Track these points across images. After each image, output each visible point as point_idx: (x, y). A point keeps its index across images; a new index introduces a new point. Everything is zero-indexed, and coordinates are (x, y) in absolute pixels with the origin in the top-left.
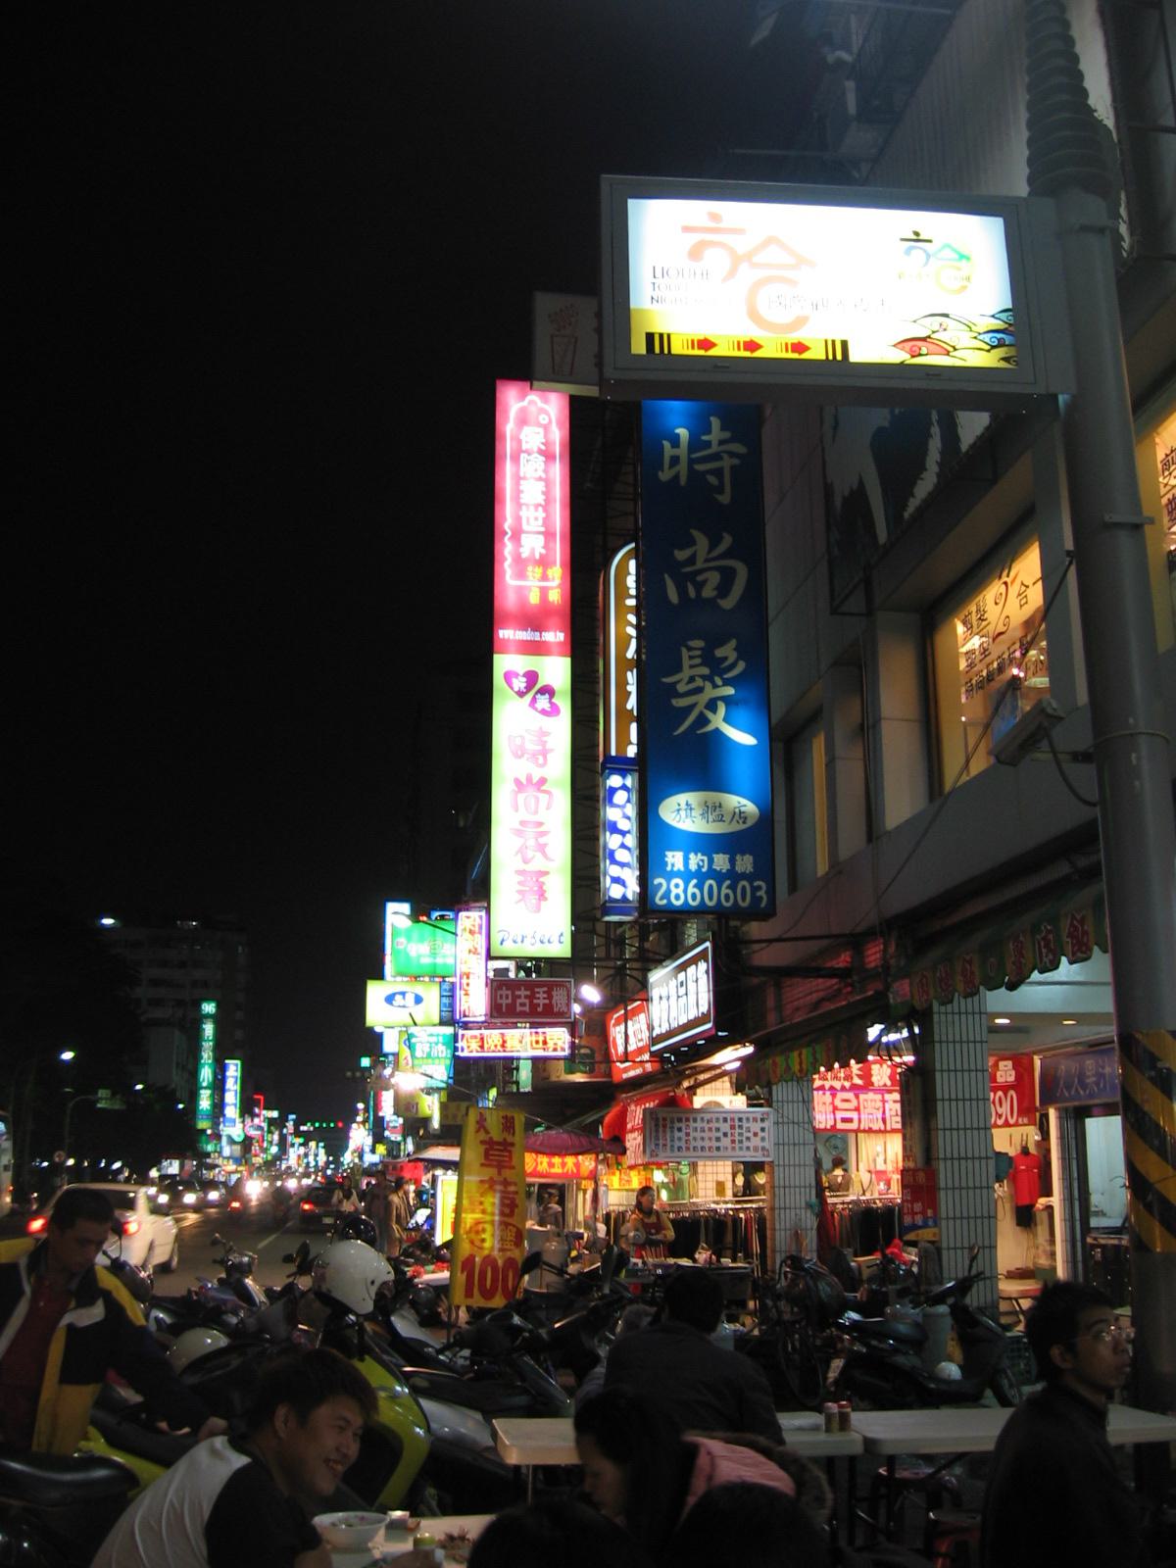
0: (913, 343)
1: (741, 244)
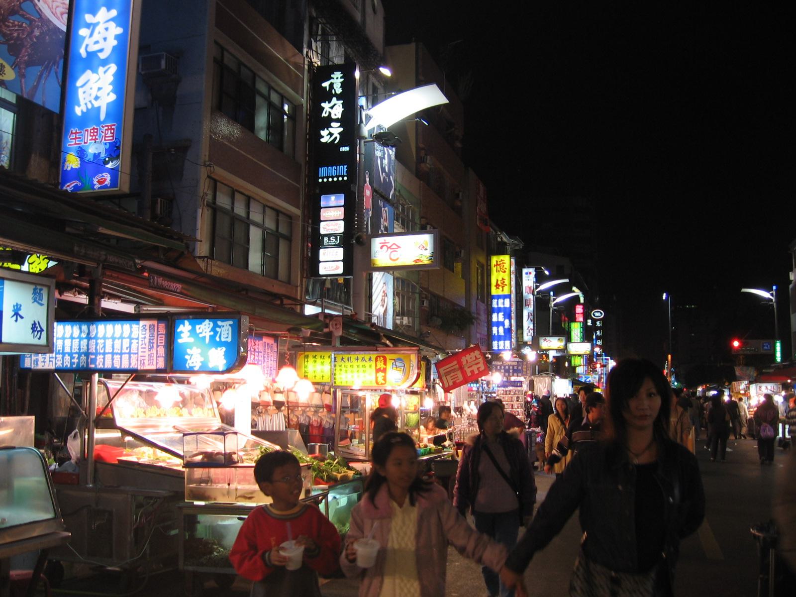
0: (416, 261)
1: (389, 245)
